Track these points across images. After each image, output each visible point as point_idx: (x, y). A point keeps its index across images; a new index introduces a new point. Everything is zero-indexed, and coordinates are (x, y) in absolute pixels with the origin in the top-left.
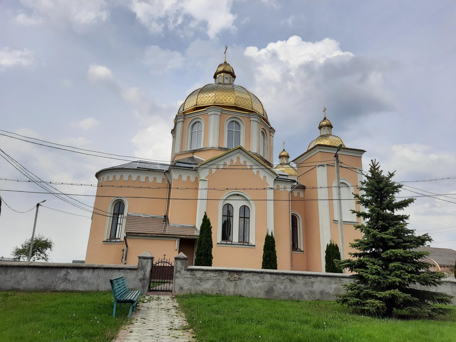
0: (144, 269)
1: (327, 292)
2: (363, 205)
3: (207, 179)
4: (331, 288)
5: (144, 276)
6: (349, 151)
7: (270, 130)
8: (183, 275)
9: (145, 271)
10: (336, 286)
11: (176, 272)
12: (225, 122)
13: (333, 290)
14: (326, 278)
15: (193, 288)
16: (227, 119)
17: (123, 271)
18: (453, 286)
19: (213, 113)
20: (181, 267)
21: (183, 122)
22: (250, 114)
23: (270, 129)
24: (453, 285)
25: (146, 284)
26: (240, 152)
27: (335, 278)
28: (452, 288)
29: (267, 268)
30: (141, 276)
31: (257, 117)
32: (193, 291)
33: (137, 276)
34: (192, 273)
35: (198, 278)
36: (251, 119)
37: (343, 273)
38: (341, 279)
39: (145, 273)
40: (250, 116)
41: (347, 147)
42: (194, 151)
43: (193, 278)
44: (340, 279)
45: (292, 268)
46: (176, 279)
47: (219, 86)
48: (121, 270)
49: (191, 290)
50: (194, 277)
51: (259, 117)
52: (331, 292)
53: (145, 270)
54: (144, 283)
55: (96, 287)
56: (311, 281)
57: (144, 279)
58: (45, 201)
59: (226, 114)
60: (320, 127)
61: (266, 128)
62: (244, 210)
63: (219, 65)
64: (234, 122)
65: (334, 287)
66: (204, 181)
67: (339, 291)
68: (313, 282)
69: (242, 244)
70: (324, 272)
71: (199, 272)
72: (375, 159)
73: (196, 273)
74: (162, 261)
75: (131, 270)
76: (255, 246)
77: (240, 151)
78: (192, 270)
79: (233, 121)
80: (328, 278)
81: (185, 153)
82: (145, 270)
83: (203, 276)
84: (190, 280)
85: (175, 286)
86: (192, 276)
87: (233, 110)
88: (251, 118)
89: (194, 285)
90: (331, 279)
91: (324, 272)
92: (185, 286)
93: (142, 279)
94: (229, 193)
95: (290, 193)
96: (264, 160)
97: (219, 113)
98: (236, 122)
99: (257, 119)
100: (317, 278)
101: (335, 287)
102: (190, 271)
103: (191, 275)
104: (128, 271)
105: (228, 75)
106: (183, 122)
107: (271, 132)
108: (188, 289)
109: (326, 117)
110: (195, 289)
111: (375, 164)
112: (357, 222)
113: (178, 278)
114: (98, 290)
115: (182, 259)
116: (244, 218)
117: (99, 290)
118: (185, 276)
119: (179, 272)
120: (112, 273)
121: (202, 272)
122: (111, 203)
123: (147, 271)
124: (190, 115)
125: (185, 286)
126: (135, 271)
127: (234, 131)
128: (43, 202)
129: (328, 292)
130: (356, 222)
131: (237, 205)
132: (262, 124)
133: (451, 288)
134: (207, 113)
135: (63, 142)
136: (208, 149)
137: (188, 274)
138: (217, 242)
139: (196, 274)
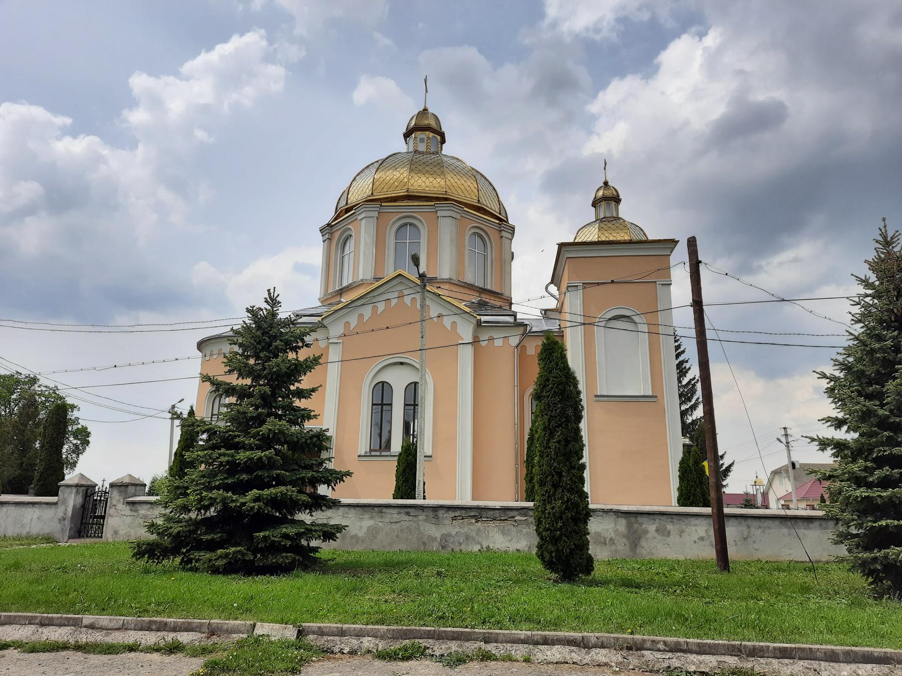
0: (66, 503)
1: (354, 535)
4: (361, 527)
5: (65, 514)
6: (617, 246)
7: (500, 228)
8: (119, 511)
9: (67, 507)
10: (371, 523)
11: (110, 507)
13: (365, 530)
14: (355, 509)
15: (133, 533)
17: (38, 506)
18: (620, 519)
19: (363, 215)
21: (330, 239)
22: (436, 205)
23: (499, 226)
24: (618, 517)
25: (66, 526)
26: (403, 283)
28: (616, 524)
30: (60, 514)
31: (451, 208)
32: (133, 536)
33: (55, 515)
34: (133, 508)
35: (141, 516)
36: (439, 214)
37: (415, 499)
39: (66, 510)
40: (437, 209)
41: (650, 238)
43: (134, 515)
46: (110, 518)
47: (416, 157)
48: (36, 505)
49: (129, 536)
50: (136, 514)
52: (360, 535)
53: (67, 504)
54: (64, 525)
55: (3, 531)
56: (327, 516)
57: (64, 519)
59: (385, 213)
60: (595, 204)
61: (487, 224)
62: (413, 389)
64: (408, 226)
65: (367, 526)
67: (376, 533)
69: (378, 454)
70: (674, 507)
71: (144, 506)
72: (274, 288)
73: (139, 508)
74: (100, 490)
76: (431, 456)
77: (403, 281)
78: (134, 503)
79: (405, 225)
81: (463, 285)
82: (67, 504)
84: (129, 519)
85: (107, 529)
86: (132, 513)
87: (403, 204)
88: (438, 211)
90: (363, 509)
91: (674, 507)
92: (122, 530)
94: (383, 362)
95: (516, 350)
97: (376, 214)
98: (411, 224)
100: (339, 509)
102: (131, 504)
103: (131, 510)
104: (44, 506)
105: (424, 134)
106: (330, 239)
108: (126, 534)
109: (608, 180)
111: (273, 296)
114: (5, 536)
115: (120, 486)
116: (382, 405)
117: (6, 536)
118: (123, 513)
120: (24, 509)
121: (149, 506)
125: (122, 530)
126: (54, 507)
128: (179, 402)
129: (356, 534)
130: (651, 394)
132: (475, 220)
133: (613, 523)
134: (355, 218)
137: (126, 510)
139: (139, 510)
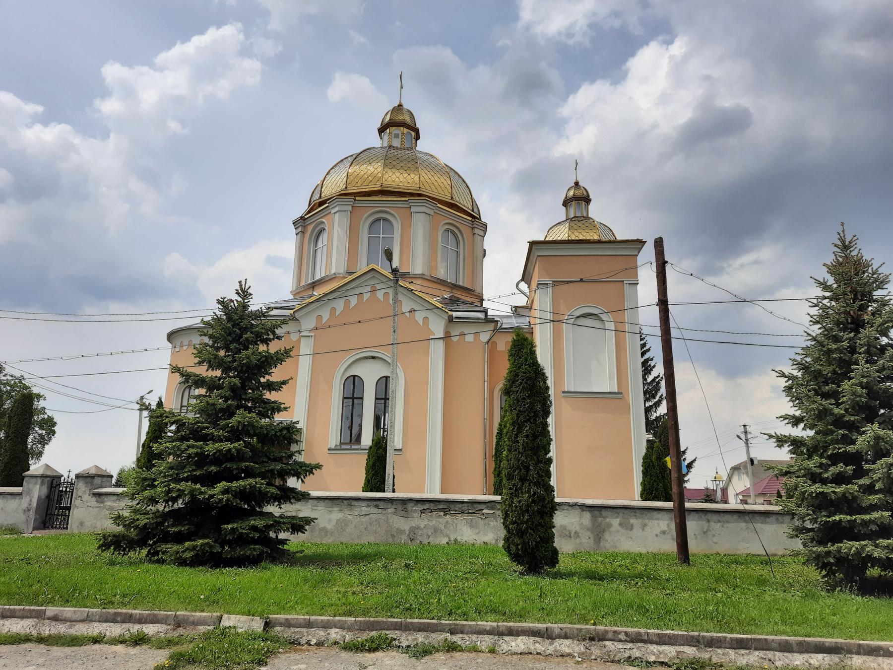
1: (323, 528)
2: (216, 370)
3: (313, 334)
4: (330, 520)
7: (473, 225)
10: (340, 515)
11: (76, 498)
12: (362, 222)
13: (334, 523)
14: (324, 502)
16: (365, 216)
20: (84, 489)
21: (303, 232)
25: (31, 517)
27: (340, 501)
28: (581, 518)
29: (653, 500)
31: (425, 204)
34: (99, 500)
35: (107, 508)
36: (413, 209)
38: (351, 503)
40: (410, 204)
42: (314, 285)
44: (349, 503)
45: (443, 492)
49: (95, 527)
51: (427, 202)
52: (329, 527)
53: (32, 495)
57: (29, 510)
58: (152, 391)
60: (565, 204)
63: (413, 115)
66: (308, 338)
68: (299, 510)
69: (348, 447)
70: (638, 502)
73: (106, 499)
74: (66, 481)
75: (13, 496)
76: (401, 450)
80: (328, 501)
83: (115, 504)
86: (98, 505)
89: (101, 518)
93: (27, 509)
96: (450, 285)
97: (350, 208)
99: (424, 207)
101: (339, 518)
103: (97, 502)
104: (9, 497)
106: (303, 232)
107: (475, 227)
110: (102, 525)
112: (620, 391)
113: (78, 508)
115: (86, 477)
119: (80, 498)
122: (176, 388)
123: (35, 497)
124: (312, 218)
126: (18, 497)
127: (381, 238)
128: (148, 393)
129: (325, 527)
131: (370, 375)
132: (442, 214)
135: (538, 260)
136: (330, 278)
137: (93, 501)
138: (329, 447)
